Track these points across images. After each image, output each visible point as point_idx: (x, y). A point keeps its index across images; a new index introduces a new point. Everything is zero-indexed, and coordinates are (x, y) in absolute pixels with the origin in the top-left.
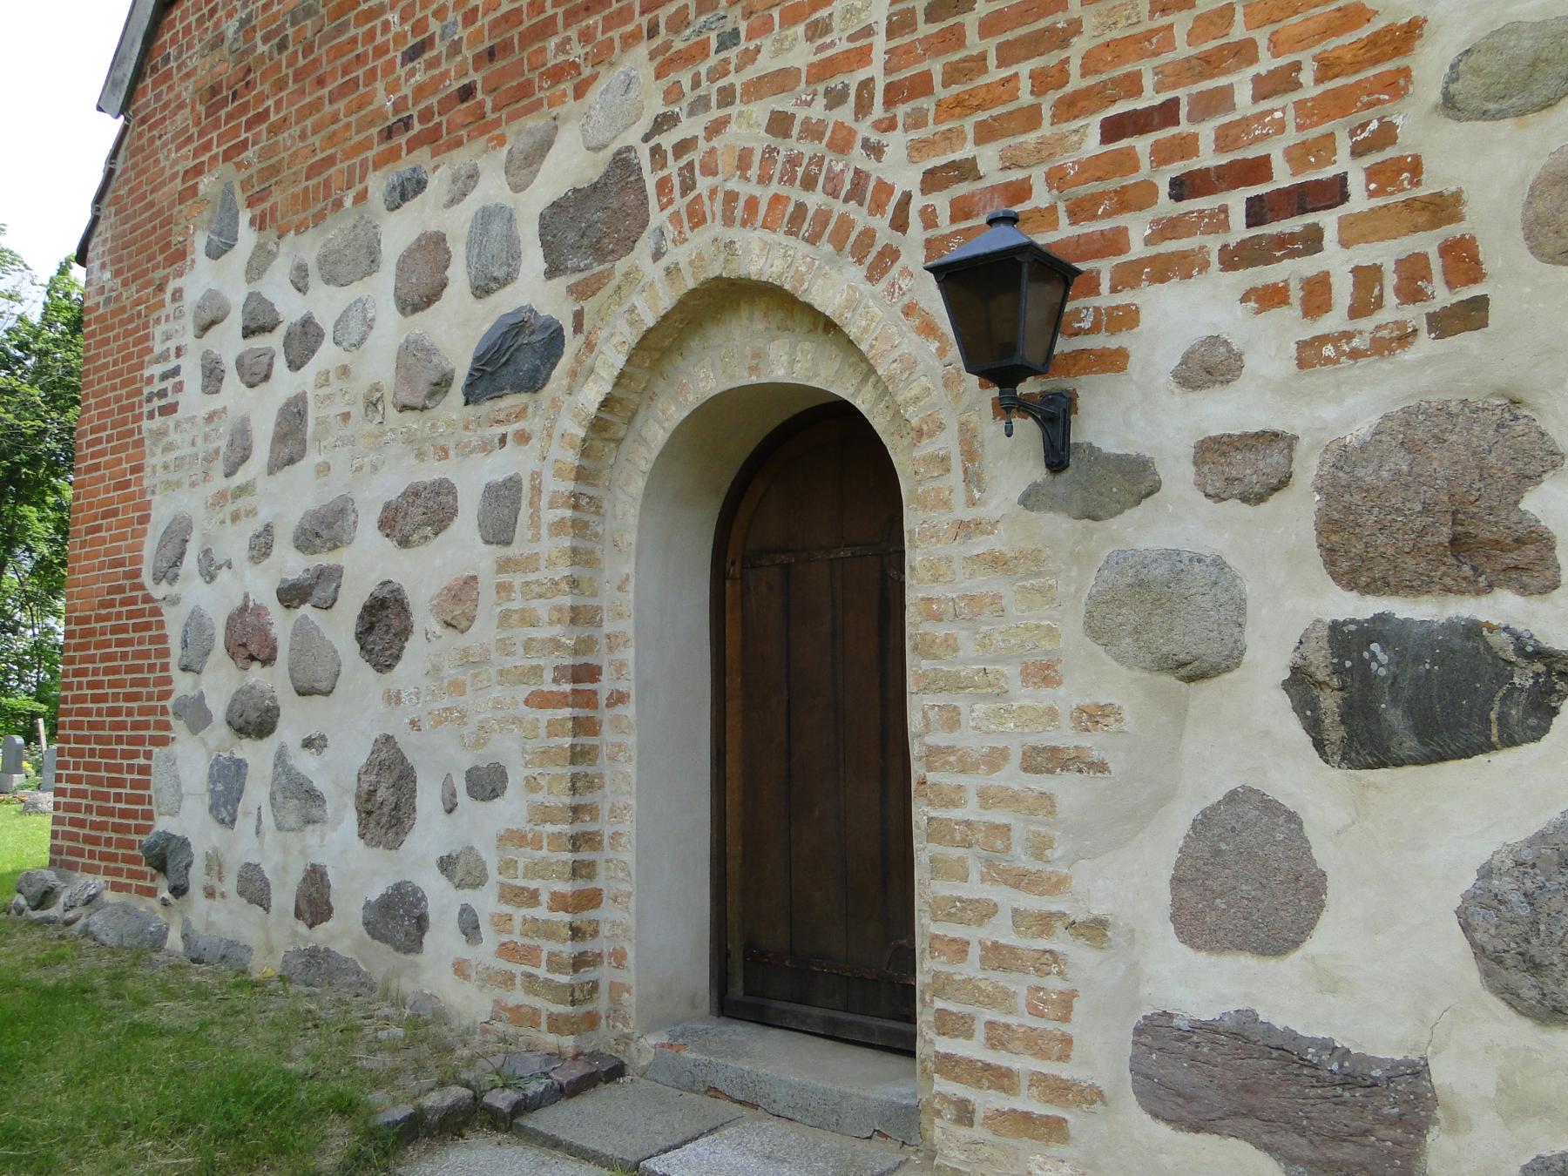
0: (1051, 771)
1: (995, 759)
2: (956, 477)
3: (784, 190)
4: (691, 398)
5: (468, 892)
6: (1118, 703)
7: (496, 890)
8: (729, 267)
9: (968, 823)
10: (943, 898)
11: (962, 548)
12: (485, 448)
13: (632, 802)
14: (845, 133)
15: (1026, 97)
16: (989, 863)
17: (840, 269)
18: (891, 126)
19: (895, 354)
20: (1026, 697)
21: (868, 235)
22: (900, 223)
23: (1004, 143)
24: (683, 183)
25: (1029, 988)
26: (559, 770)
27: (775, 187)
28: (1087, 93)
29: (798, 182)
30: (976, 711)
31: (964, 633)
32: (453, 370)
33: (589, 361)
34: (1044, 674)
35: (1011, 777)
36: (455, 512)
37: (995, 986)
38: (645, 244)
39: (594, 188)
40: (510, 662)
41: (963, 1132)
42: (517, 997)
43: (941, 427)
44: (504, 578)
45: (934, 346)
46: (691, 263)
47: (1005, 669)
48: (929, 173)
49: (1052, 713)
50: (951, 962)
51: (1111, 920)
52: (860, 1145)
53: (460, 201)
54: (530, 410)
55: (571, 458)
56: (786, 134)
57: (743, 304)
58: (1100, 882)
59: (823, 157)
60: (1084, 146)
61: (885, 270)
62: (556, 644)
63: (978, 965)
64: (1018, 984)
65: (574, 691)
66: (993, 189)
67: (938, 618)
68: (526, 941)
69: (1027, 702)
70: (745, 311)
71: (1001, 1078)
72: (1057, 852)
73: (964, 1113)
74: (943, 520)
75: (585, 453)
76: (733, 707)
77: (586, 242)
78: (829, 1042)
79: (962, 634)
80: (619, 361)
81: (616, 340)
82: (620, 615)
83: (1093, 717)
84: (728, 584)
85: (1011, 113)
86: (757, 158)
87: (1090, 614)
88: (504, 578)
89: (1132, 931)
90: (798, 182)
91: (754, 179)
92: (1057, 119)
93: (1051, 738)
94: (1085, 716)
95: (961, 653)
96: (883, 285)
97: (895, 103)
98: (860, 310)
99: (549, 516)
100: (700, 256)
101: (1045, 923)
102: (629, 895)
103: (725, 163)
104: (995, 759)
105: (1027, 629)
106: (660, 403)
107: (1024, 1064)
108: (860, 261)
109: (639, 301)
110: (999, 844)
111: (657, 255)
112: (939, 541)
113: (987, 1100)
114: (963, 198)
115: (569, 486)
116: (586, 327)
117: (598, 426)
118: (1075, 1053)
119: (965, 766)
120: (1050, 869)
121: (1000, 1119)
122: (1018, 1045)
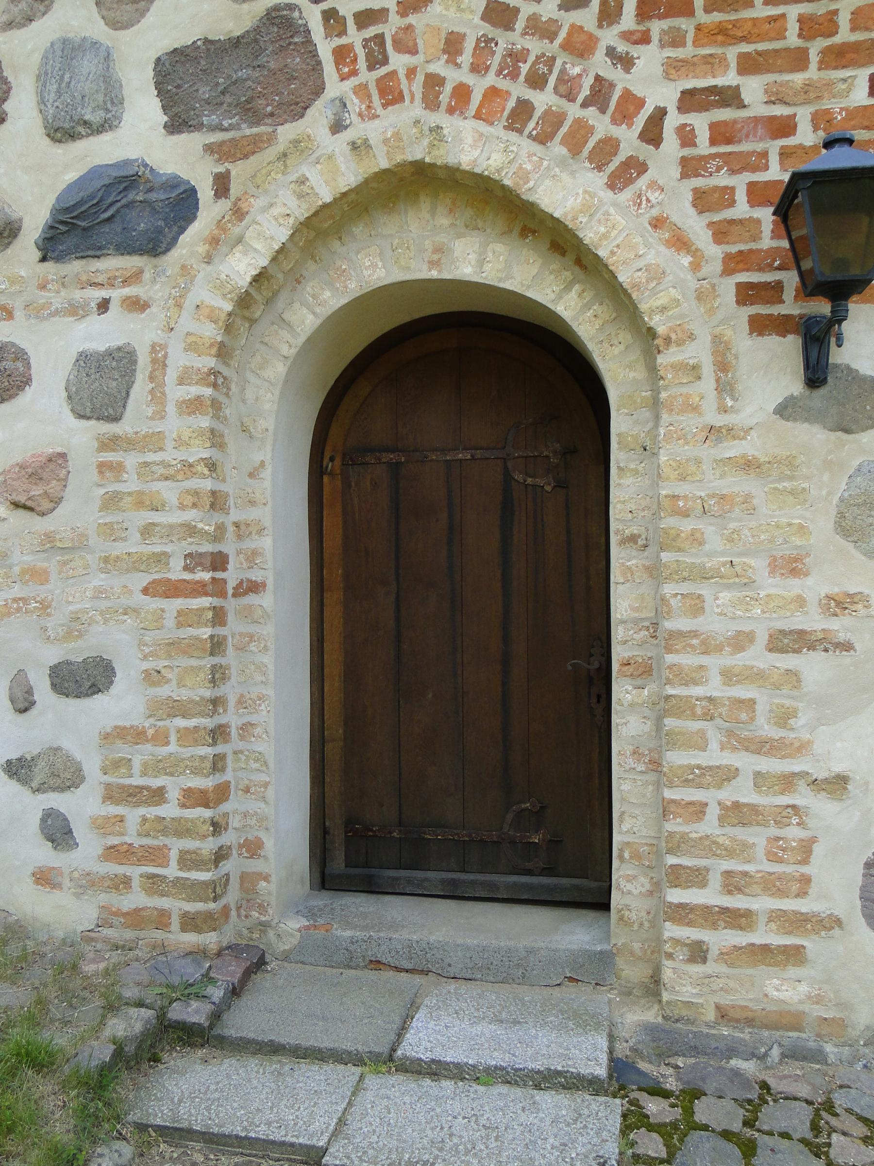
0: (797, 651)
1: (741, 641)
2: (708, 384)
3: (503, 84)
4: (352, 285)
5: (52, 795)
6: (866, 591)
7: (100, 791)
8: (435, 152)
9: (710, 699)
10: (681, 767)
11: (712, 451)
12: (75, 311)
13: (270, 692)
14: (583, 37)
15: (792, 39)
16: (730, 733)
17: (573, 173)
18: (644, 39)
19: (641, 263)
20: (772, 586)
21: (609, 146)
22: (652, 134)
23: (770, 78)
24: (369, 56)
25: (769, 839)
26: (194, 662)
27: (491, 79)
28: (855, 47)
29: (522, 78)
30: (720, 599)
31: (713, 528)
32: (21, 220)
33: (236, 230)
34: (793, 566)
35: (757, 657)
36: (27, 381)
37: (733, 839)
38: (318, 116)
39: (236, 43)
40: (118, 549)
41: (696, 969)
42: (136, 899)
43: (692, 337)
44: (109, 457)
45: (686, 260)
46: (386, 141)
47: (752, 562)
48: (687, 94)
49: (800, 602)
50: (686, 823)
51: (851, 775)
52: (556, 992)
53: (22, 26)
54: (147, 276)
55: (211, 332)
56: (508, 26)
57: (423, 197)
58: (839, 745)
59: (554, 59)
60: (852, 95)
61: (630, 181)
62: (191, 530)
63: (716, 823)
64: (757, 837)
65: (213, 579)
66: (756, 120)
67: (685, 514)
68: (146, 841)
69: (772, 591)
70: (425, 204)
71: (738, 919)
72: (802, 720)
73: (698, 953)
74: (691, 423)
75: (228, 329)
76: (334, 599)
77: (228, 99)
78: (448, 901)
79: (709, 530)
80: (282, 234)
81: (277, 211)
82: (253, 503)
83: (840, 604)
84: (326, 479)
85: (776, 51)
86: (469, 45)
87: (841, 515)
88: (109, 457)
89: (867, 783)
90: (522, 78)
91: (466, 66)
92: (823, 65)
93: (798, 622)
94: (833, 604)
95: (707, 547)
96: (627, 195)
97: (650, 18)
98: (599, 215)
99: (176, 393)
100: (397, 136)
101: (788, 782)
102: (266, 785)
103: (428, 43)
104: (741, 641)
105: (778, 526)
106: (309, 288)
107: (761, 904)
108: (599, 168)
109: (315, 176)
110: (744, 716)
111: (337, 127)
112: (687, 443)
113: (720, 939)
114: (724, 123)
115: (209, 362)
116: (235, 190)
117: (244, 301)
118: (813, 890)
119: (707, 648)
120: (794, 736)
121: (733, 956)
122: (756, 889)
